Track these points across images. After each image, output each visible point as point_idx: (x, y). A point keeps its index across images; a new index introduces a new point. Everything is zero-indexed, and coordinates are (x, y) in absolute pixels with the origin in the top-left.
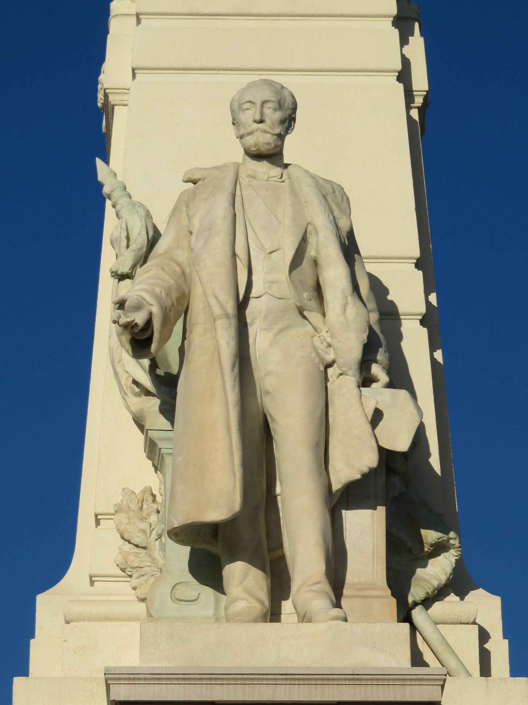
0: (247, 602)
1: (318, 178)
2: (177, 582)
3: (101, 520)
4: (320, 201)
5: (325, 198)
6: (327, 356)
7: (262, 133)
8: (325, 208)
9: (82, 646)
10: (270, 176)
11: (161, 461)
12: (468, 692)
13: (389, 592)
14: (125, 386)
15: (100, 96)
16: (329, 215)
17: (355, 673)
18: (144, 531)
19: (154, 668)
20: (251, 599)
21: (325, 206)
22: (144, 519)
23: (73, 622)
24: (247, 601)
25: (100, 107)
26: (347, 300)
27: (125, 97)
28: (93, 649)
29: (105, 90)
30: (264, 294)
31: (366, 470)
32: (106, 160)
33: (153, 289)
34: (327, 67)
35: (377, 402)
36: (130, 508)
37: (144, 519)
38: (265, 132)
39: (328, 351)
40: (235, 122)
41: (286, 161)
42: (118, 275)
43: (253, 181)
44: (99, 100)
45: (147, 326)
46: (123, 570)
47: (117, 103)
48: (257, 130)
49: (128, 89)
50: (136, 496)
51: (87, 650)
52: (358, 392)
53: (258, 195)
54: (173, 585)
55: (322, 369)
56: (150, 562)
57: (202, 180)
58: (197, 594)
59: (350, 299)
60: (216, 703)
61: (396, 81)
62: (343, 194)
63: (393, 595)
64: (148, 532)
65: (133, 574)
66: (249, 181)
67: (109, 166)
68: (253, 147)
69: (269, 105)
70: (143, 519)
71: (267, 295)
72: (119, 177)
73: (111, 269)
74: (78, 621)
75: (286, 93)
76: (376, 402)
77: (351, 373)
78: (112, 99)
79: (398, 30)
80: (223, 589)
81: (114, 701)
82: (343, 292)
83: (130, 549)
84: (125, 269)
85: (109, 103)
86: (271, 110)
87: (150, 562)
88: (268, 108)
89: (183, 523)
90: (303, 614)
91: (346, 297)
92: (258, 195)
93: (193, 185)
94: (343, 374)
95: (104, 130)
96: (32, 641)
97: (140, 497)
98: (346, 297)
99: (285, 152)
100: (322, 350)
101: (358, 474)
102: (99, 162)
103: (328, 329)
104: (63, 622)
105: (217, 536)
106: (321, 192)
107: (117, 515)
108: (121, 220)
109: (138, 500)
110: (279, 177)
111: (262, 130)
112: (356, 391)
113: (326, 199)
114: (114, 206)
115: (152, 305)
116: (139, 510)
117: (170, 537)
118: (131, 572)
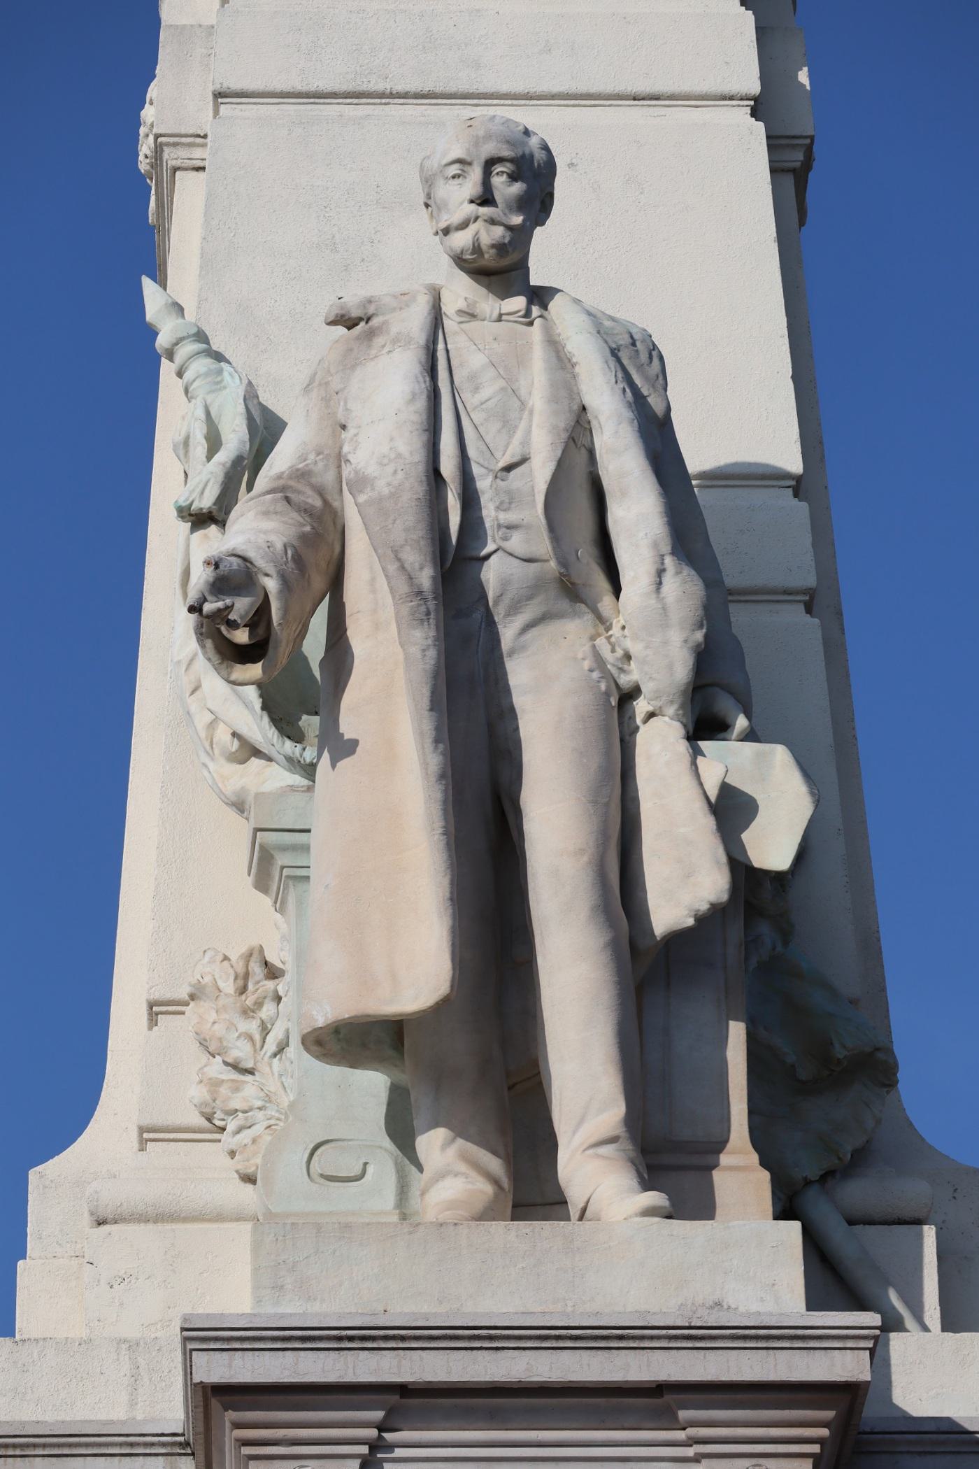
0: (464, 1180)
1: (599, 315)
2: (318, 1140)
3: (159, 1016)
4: (607, 362)
5: (614, 353)
6: (622, 676)
7: (488, 225)
8: (616, 376)
9: (126, 1273)
10: (502, 312)
11: (283, 893)
12: (919, 1364)
13: (754, 1158)
14: (207, 740)
15: (146, 147)
16: (624, 390)
17: (692, 1324)
18: (250, 1038)
19: (283, 1316)
20: (473, 1174)
21: (616, 372)
22: (249, 1012)
23: (107, 1223)
24: (467, 1178)
25: (143, 171)
26: (663, 564)
27: (197, 153)
28: (148, 1278)
29: (157, 137)
30: (495, 551)
31: (704, 907)
32: (161, 279)
33: (268, 542)
34: (610, 88)
35: (727, 771)
36: (219, 989)
37: (249, 1012)
38: (492, 222)
39: (626, 667)
40: (429, 202)
41: (534, 281)
42: (191, 515)
43: (469, 321)
44: (141, 158)
45: (256, 618)
46: (209, 1120)
47: (182, 163)
48: (476, 219)
49: (205, 137)
50: (230, 964)
51: (136, 1283)
52: (688, 750)
53: (479, 350)
54: (311, 1146)
55: (614, 701)
56: (263, 1100)
57: (365, 320)
58: (361, 1166)
59: (669, 561)
60: (410, 1387)
61: (750, 116)
62: (652, 348)
63: (764, 1163)
64: (257, 1038)
65: (226, 1125)
66: (461, 322)
67: (165, 289)
68: (469, 252)
69: (499, 168)
70: (247, 1012)
71: (500, 553)
72: (190, 315)
73: (176, 502)
74: (116, 1223)
75: (534, 142)
76: (725, 770)
77: (671, 710)
78: (171, 157)
79: (753, 13)
80: (416, 1152)
81: (203, 1385)
82: (655, 545)
83: (221, 1073)
84: (206, 502)
85: (165, 164)
86: (504, 178)
87: (263, 1100)
88: (497, 174)
89: (334, 1020)
90: (582, 1205)
91: (662, 556)
92: (479, 350)
93: (346, 330)
94: (657, 712)
95: (151, 219)
96: (21, 1263)
97: (240, 969)
98: (662, 556)
99: (532, 263)
100: (614, 665)
101: (690, 916)
102: (148, 285)
103: (626, 622)
104: (86, 1220)
105: (403, 1045)
106: (606, 342)
107: (192, 1004)
108: (193, 401)
109: (236, 973)
110: (522, 313)
111: (486, 218)
112: (683, 747)
113: (619, 360)
114: (180, 374)
115: (267, 575)
116: (237, 994)
117: (307, 1049)
118: (223, 1120)
